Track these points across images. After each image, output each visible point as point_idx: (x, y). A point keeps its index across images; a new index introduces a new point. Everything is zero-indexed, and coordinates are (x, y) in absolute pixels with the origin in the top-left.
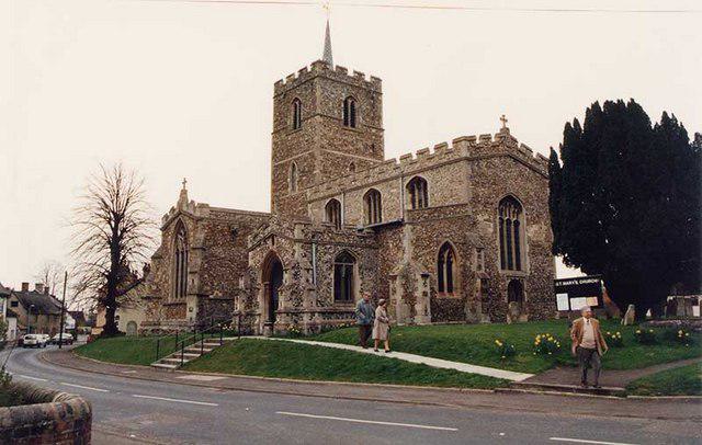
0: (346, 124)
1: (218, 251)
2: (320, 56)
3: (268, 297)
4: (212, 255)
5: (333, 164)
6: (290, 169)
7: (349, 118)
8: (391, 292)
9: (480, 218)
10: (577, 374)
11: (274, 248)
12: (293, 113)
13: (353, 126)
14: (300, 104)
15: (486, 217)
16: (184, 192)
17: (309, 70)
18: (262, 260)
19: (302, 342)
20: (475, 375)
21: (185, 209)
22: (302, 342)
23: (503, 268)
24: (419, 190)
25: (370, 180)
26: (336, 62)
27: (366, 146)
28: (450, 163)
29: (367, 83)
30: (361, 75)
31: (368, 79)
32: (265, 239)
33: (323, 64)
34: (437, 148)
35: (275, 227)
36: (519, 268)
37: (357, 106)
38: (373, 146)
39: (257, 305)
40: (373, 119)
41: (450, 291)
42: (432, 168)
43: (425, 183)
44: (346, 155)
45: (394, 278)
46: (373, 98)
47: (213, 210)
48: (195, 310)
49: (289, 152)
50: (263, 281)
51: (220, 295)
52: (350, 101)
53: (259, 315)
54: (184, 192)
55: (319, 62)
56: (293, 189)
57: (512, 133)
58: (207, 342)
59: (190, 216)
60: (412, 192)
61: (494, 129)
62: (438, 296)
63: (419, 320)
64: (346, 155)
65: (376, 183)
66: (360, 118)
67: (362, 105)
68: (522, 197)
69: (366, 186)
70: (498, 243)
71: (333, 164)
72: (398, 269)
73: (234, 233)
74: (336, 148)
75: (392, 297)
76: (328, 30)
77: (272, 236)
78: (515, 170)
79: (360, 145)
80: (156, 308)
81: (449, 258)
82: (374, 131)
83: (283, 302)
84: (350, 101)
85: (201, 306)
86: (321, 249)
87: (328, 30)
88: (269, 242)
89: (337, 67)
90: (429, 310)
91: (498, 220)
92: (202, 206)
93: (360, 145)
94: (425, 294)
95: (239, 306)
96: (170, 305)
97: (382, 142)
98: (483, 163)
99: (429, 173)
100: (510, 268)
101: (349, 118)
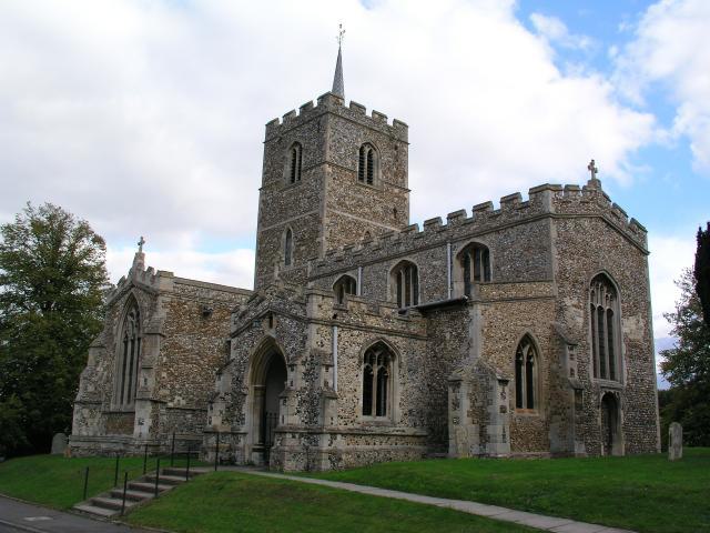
0: (361, 178)
1: (184, 341)
2: (329, 88)
3: (258, 408)
4: (174, 345)
5: (343, 230)
6: (284, 236)
7: (366, 172)
8: (450, 406)
9: (568, 302)
10: (170, 462)
11: (272, 333)
12: (290, 162)
13: (370, 182)
14: (301, 149)
15: (575, 302)
16: (139, 256)
17: (315, 105)
18: (252, 352)
19: (319, 482)
20: (392, 499)
21: (139, 279)
22: (319, 482)
23: (595, 376)
24: (476, 262)
25: (402, 248)
26: (350, 96)
27: (386, 209)
28: (525, 222)
29: (389, 127)
30: (382, 116)
31: (390, 123)
32: (259, 318)
33: (332, 99)
34: (505, 201)
35: (274, 302)
36: (612, 378)
37: (375, 156)
38: (395, 211)
39: (241, 419)
40: (396, 175)
41: (530, 406)
42: (497, 230)
43: (486, 252)
44: (361, 219)
45: (457, 383)
46: (396, 148)
47: (179, 281)
48: (148, 422)
49: (283, 211)
50: (254, 381)
51: (183, 402)
52: (367, 150)
53: (245, 434)
54: (139, 256)
55: (328, 95)
56: (288, 262)
57: (605, 188)
58: (165, 473)
59: (147, 290)
60: (465, 264)
61: (581, 179)
62: (515, 412)
63: (502, 449)
64: (361, 219)
65: (409, 253)
66: (378, 174)
67: (383, 156)
68: (616, 277)
69: (395, 257)
70: (590, 342)
71: (343, 230)
72: (466, 370)
73: (206, 314)
74: (348, 209)
75: (451, 413)
76: (340, 51)
77: (270, 315)
78: (608, 238)
79: (379, 209)
80: (93, 416)
81: (529, 357)
82: (396, 191)
83: (291, 415)
84: (367, 150)
85: (155, 417)
86: (346, 335)
87: (340, 51)
88: (265, 324)
89: (352, 103)
90: (508, 434)
91: (589, 307)
92: (161, 274)
93: (379, 209)
94: (503, 410)
95: (216, 420)
96: (111, 413)
97: (407, 207)
98: (570, 224)
99: (493, 237)
100: (603, 376)
101: (366, 172)
